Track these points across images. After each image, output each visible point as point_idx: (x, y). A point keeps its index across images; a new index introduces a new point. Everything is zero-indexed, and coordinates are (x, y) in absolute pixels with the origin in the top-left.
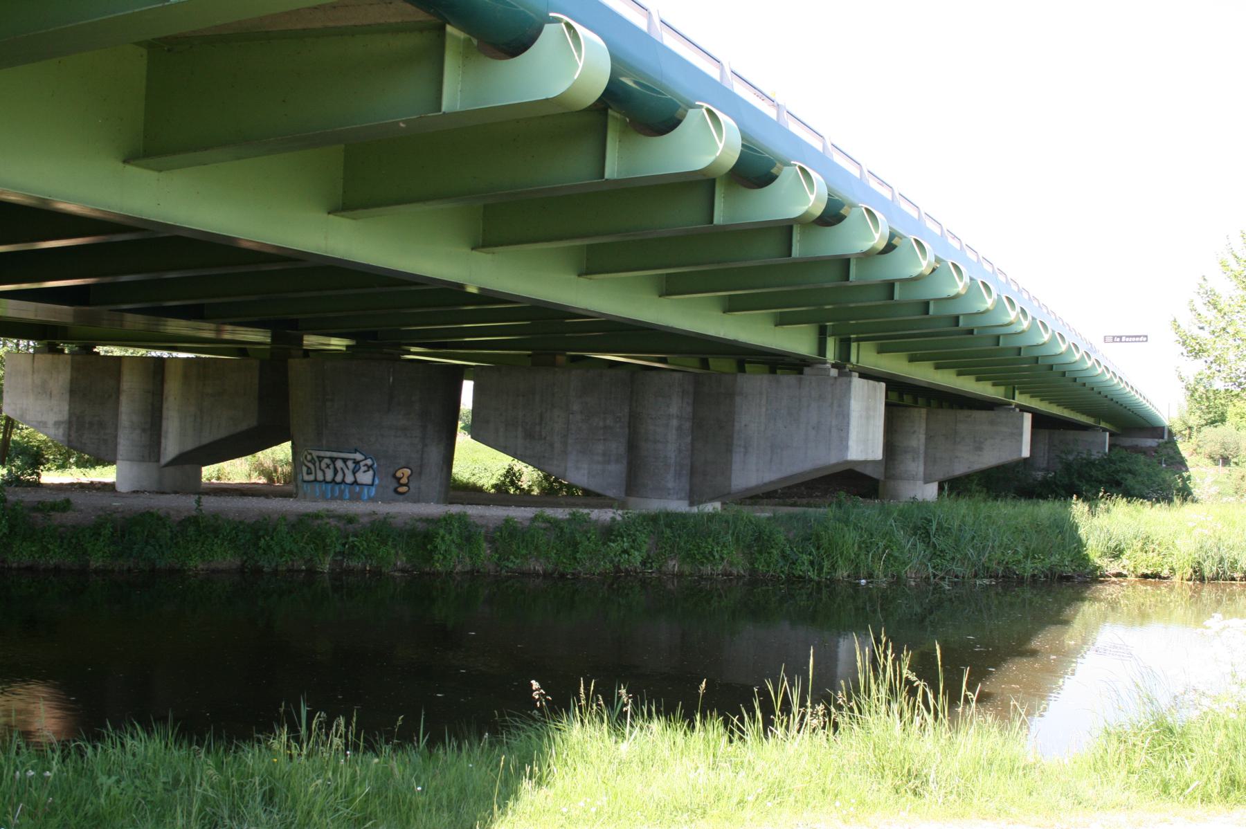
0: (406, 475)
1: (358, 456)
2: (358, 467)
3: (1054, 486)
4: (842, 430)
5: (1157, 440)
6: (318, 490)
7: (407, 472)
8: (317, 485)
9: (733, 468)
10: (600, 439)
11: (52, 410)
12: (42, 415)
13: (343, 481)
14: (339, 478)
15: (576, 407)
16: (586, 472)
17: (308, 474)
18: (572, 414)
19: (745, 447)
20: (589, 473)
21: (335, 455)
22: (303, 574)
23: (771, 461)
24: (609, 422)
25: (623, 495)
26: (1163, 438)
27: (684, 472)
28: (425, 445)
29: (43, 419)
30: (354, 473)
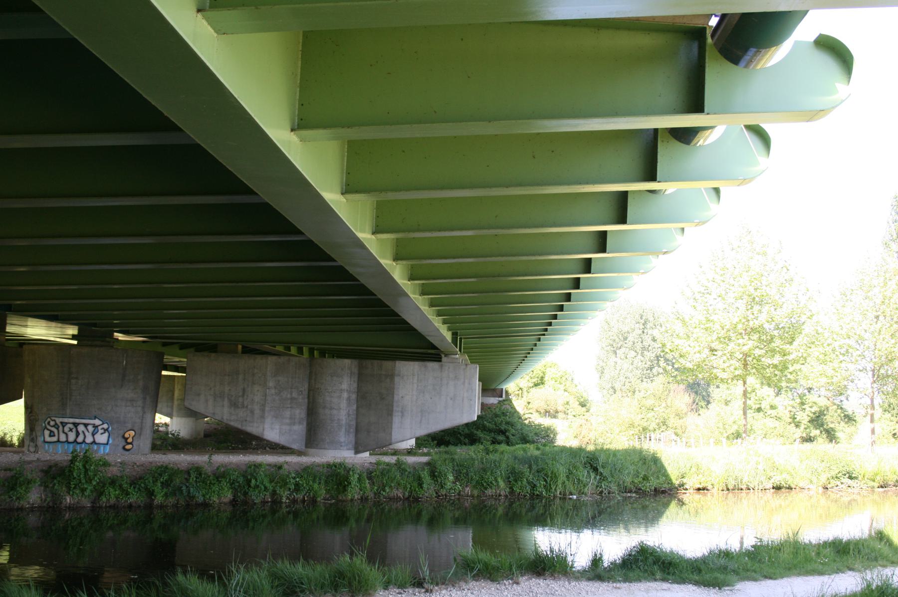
0: (131, 436)
1: (97, 422)
2: (96, 431)
3: (459, 435)
4: (471, 400)
5: (497, 398)
6: (60, 449)
7: (132, 433)
8: (60, 445)
9: (393, 426)
10: (288, 407)
13: (84, 441)
15: (271, 384)
16: (278, 431)
17: (50, 436)
18: (269, 389)
19: (402, 412)
20: (280, 432)
21: (77, 421)
22: (269, 504)
23: (421, 422)
24: (295, 395)
25: (303, 448)
26: (502, 397)
27: (352, 430)
28: (144, 412)
30: (93, 435)
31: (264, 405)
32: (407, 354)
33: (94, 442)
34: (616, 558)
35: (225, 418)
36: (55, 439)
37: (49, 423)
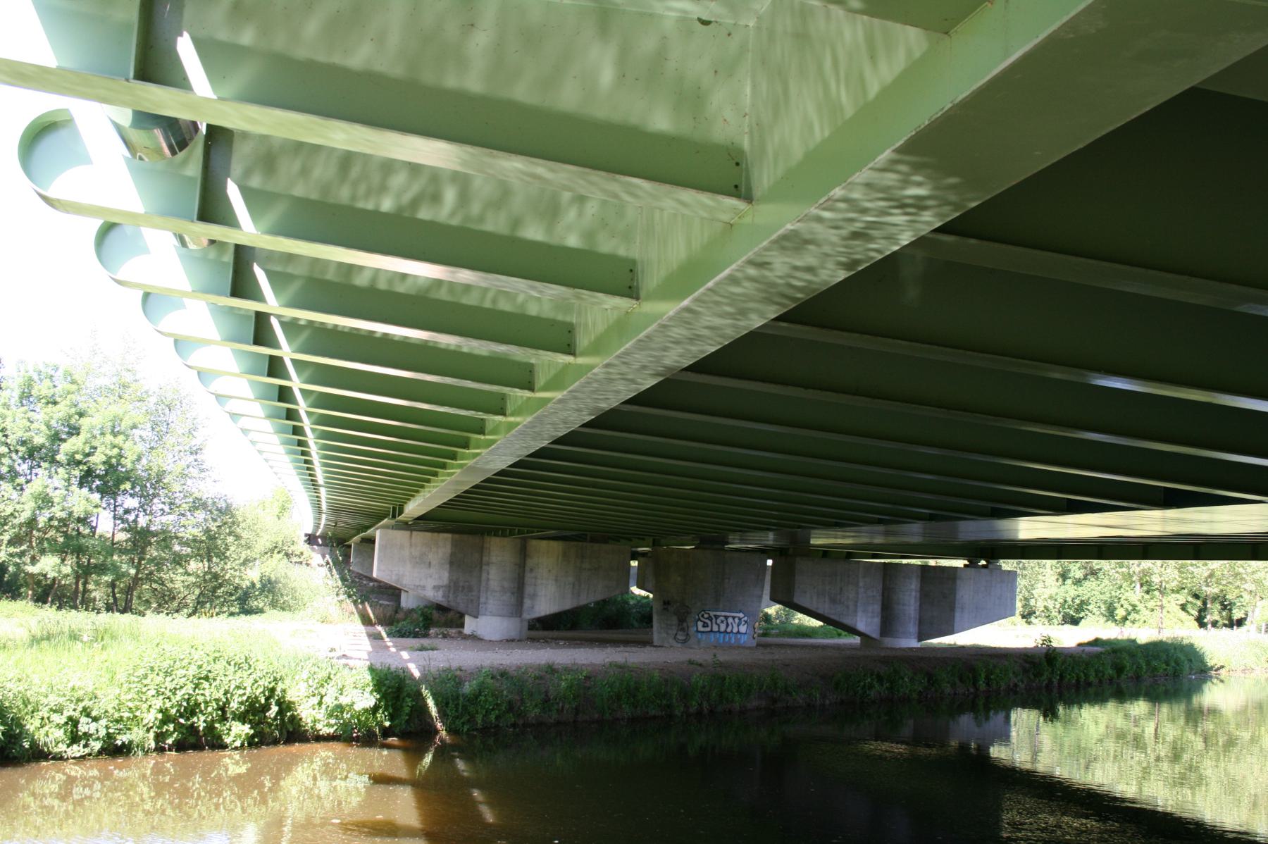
1: (741, 615)
8: (712, 635)
11: (431, 577)
12: (420, 580)
13: (732, 632)
14: (729, 630)
15: (861, 584)
17: (704, 626)
19: (962, 609)
21: (728, 614)
24: (875, 594)
29: (422, 584)
30: (738, 626)
31: (857, 602)
32: (732, 522)
33: (738, 632)
34: (298, 711)
35: (826, 611)
36: (709, 629)
37: (703, 616)
